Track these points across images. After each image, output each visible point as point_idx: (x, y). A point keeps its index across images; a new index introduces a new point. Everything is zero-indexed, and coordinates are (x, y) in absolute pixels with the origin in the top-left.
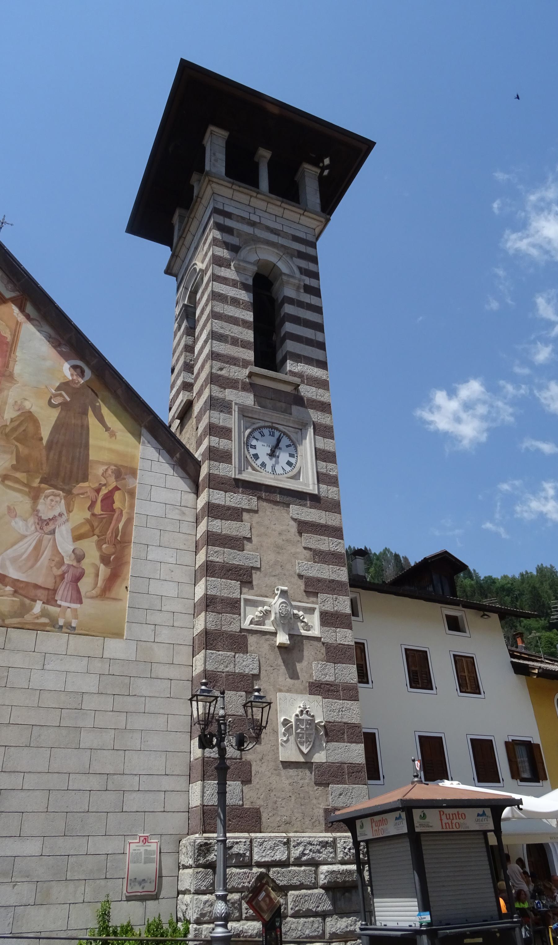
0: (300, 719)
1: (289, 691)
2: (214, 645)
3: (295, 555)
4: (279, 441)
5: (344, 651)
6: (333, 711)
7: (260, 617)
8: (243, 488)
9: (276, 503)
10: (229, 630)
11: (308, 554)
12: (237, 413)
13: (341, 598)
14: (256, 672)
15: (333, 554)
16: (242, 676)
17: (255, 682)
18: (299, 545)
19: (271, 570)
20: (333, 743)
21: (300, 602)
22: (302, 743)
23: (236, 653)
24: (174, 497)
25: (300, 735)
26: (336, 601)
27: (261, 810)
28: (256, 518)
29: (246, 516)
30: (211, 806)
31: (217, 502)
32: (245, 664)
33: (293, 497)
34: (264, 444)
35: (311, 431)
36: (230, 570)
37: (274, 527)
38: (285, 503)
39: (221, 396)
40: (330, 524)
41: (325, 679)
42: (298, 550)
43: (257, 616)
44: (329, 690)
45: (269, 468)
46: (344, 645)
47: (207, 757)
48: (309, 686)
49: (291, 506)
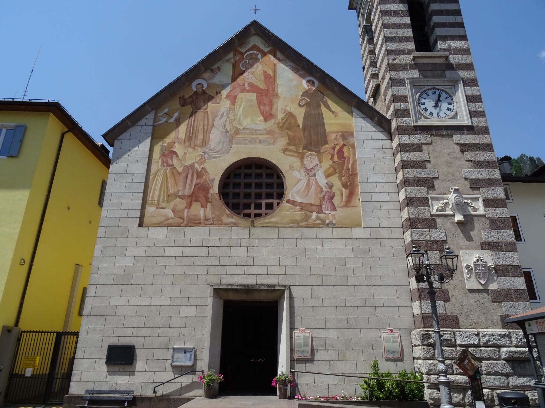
1: (467, 248)
3: (461, 166)
4: (439, 96)
7: (442, 207)
9: (443, 136)
15: (487, 162)
16: (436, 242)
18: (463, 159)
22: (480, 278)
24: (378, 144)
28: (431, 147)
29: (424, 147)
31: (405, 142)
35: (461, 84)
39: (397, 76)
45: (435, 115)
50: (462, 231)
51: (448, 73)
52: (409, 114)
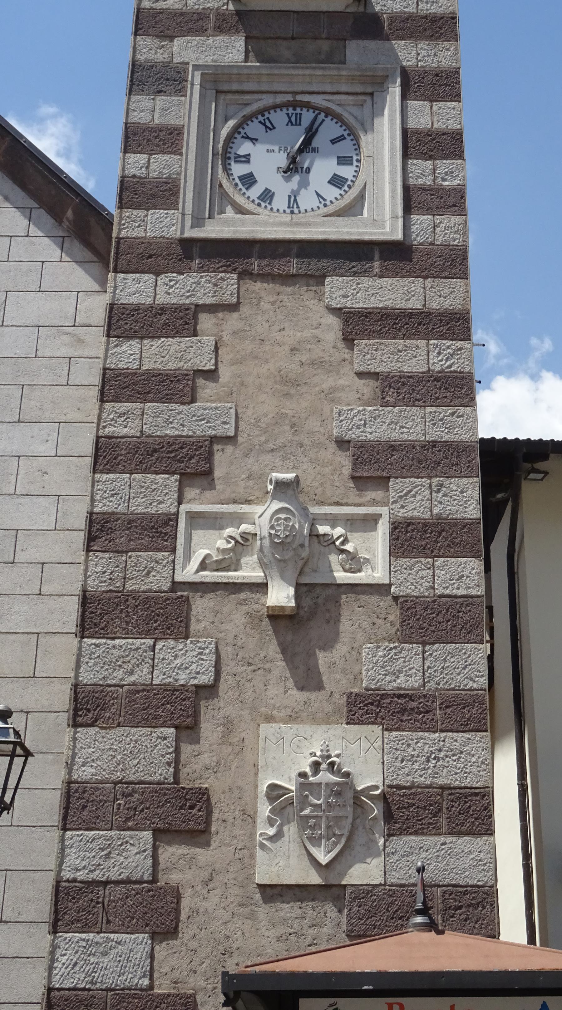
0: (311, 784)
1: (293, 718)
2: (102, 625)
3: (331, 395)
4: (311, 133)
5: (452, 612)
6: (412, 759)
7: (224, 551)
8: (201, 257)
9: (287, 279)
10: (144, 588)
11: (368, 388)
12: (197, 88)
13: (453, 484)
14: (206, 679)
15: (437, 380)
16: (171, 692)
17: (203, 703)
18: (346, 369)
19: (263, 439)
20: (405, 838)
21: (337, 504)
22: (316, 841)
23: (156, 639)
24: (56, 309)
25: (312, 822)
26: (438, 491)
27: (200, 998)
28: (232, 321)
29: (206, 322)
30: (69, 989)
31: (133, 300)
32: (181, 663)
33: (334, 256)
34: (270, 147)
35: (395, 92)
36: (155, 451)
37: (278, 336)
38: (311, 276)
39: (160, 57)
40: (435, 306)
41: (394, 684)
42: (341, 382)
43: (218, 549)
44: (403, 711)
45: (281, 202)
46: (456, 597)
47: (68, 881)
48: (348, 703)
49: (328, 279)
50: (284, 650)
51: (357, 51)
52: (176, 194)
